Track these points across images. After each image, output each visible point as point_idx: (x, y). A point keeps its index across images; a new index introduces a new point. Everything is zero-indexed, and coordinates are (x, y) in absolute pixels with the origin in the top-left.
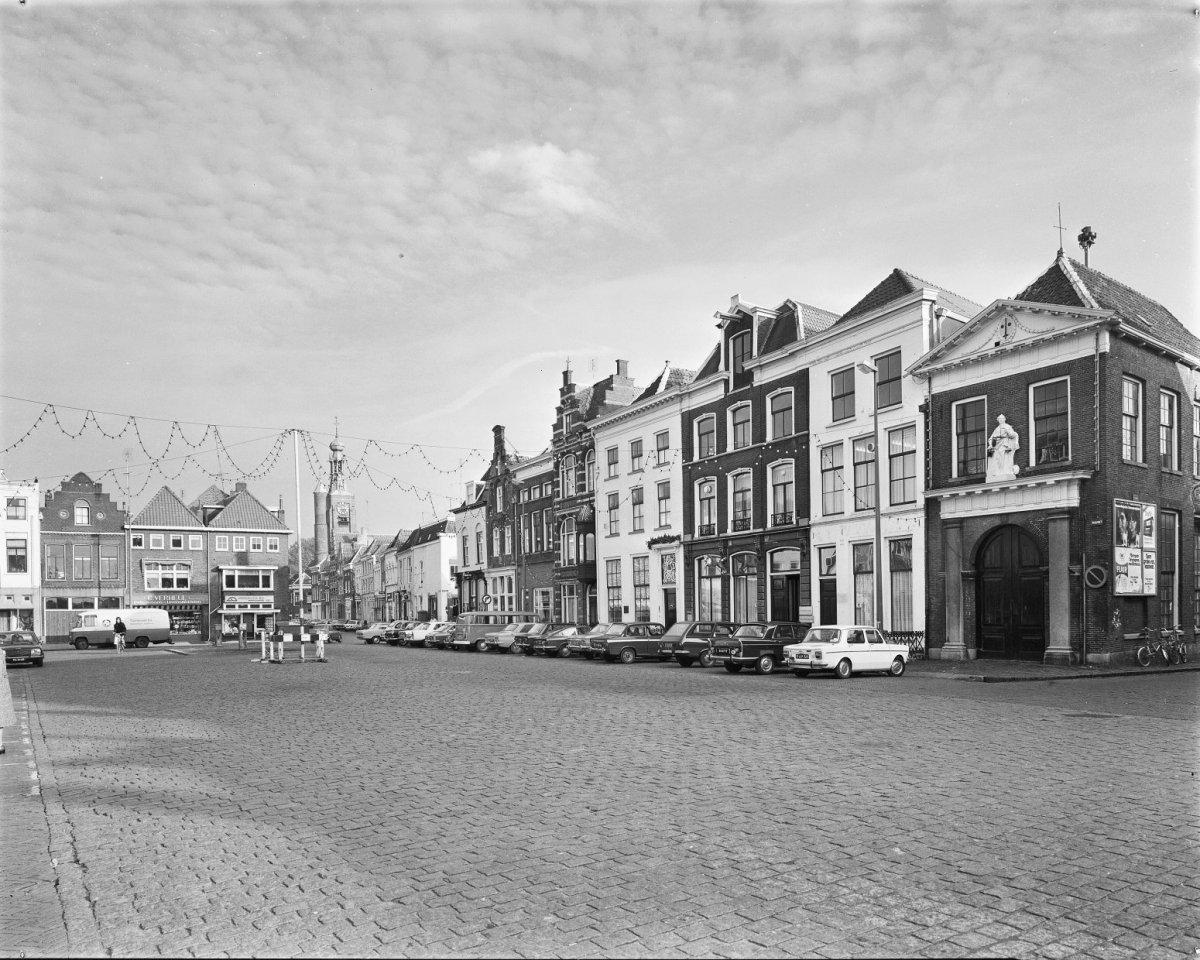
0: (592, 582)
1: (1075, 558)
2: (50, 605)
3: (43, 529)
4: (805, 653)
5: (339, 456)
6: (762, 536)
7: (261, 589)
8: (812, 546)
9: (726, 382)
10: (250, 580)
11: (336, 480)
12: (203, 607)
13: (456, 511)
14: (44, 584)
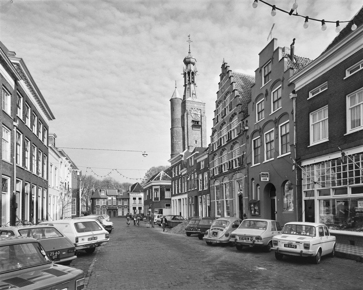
4: (294, 243)
5: (192, 68)
8: (41, 174)
11: (190, 88)
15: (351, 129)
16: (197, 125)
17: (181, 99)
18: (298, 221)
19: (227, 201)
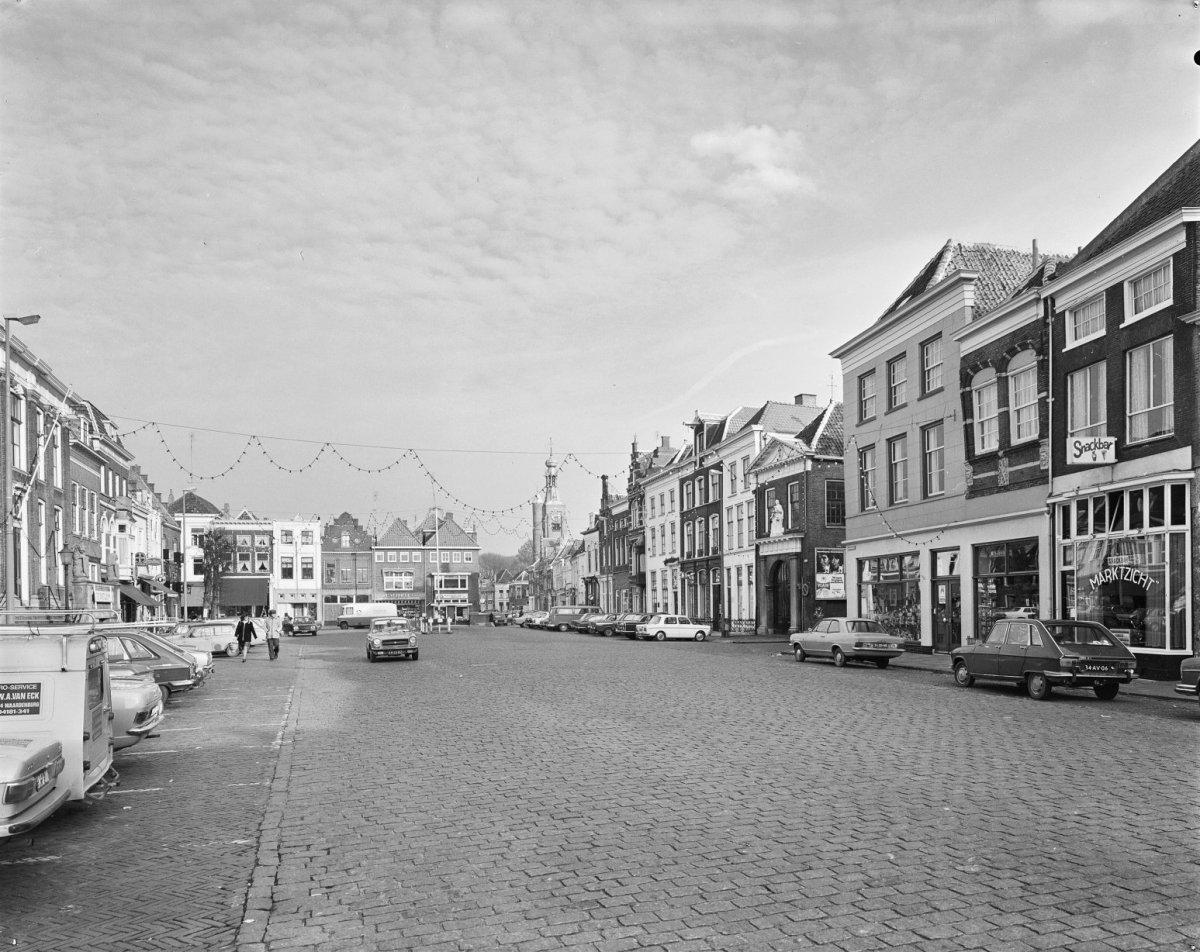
0: (643, 586)
1: (799, 580)
2: (328, 600)
3: (323, 550)
5: (553, 471)
6: (708, 560)
7: (459, 589)
9: (695, 463)
10: (451, 583)
12: (422, 601)
13: (585, 534)
14: (324, 587)
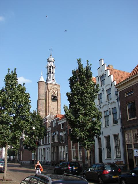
15: (114, 124)
16: (55, 99)
17: (45, 82)
18: (99, 149)
19: (73, 150)
